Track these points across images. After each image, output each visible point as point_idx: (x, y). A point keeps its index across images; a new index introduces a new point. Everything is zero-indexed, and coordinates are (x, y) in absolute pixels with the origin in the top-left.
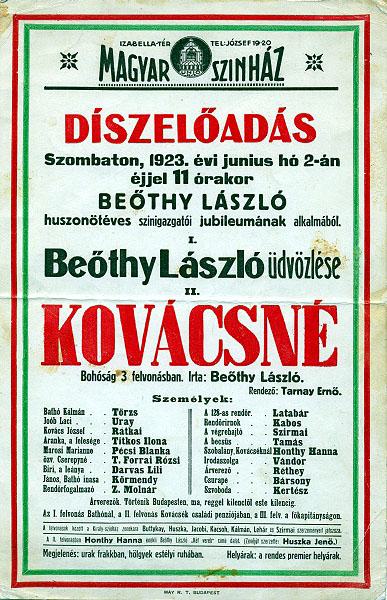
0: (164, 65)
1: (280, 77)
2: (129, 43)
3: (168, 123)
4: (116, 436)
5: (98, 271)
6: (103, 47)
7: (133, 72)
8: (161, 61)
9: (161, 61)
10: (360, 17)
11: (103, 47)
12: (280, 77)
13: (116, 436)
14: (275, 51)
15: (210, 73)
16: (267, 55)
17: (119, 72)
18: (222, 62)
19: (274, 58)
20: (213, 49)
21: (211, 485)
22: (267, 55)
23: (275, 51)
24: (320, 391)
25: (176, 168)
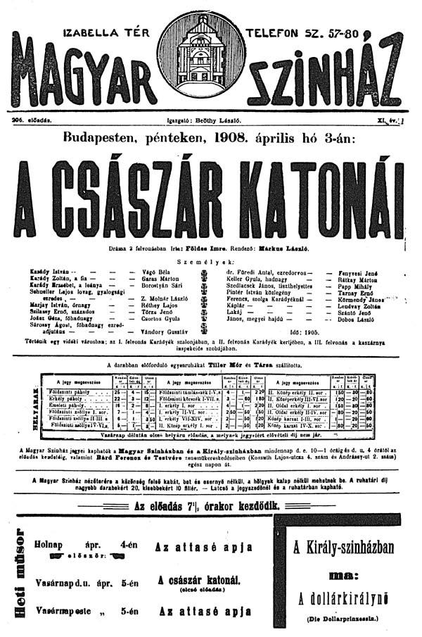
0: (141, 70)
1: (392, 95)
2: (76, 33)
3: (130, 34)
4: (144, 308)
5: (355, 33)
6: (16, 35)
7: (74, 78)
8: (136, 64)
9: (136, 64)
10: (42, 378)
11: (16, 35)
12: (392, 95)
13: (144, 308)
14: (383, 43)
15: (246, 87)
16: (367, 50)
17: (45, 78)
18: (276, 65)
19: (381, 58)
20: (250, 42)
21: (146, 283)
22: (367, 50)
23: (383, 43)
24: (325, 619)
25: (210, 396)
